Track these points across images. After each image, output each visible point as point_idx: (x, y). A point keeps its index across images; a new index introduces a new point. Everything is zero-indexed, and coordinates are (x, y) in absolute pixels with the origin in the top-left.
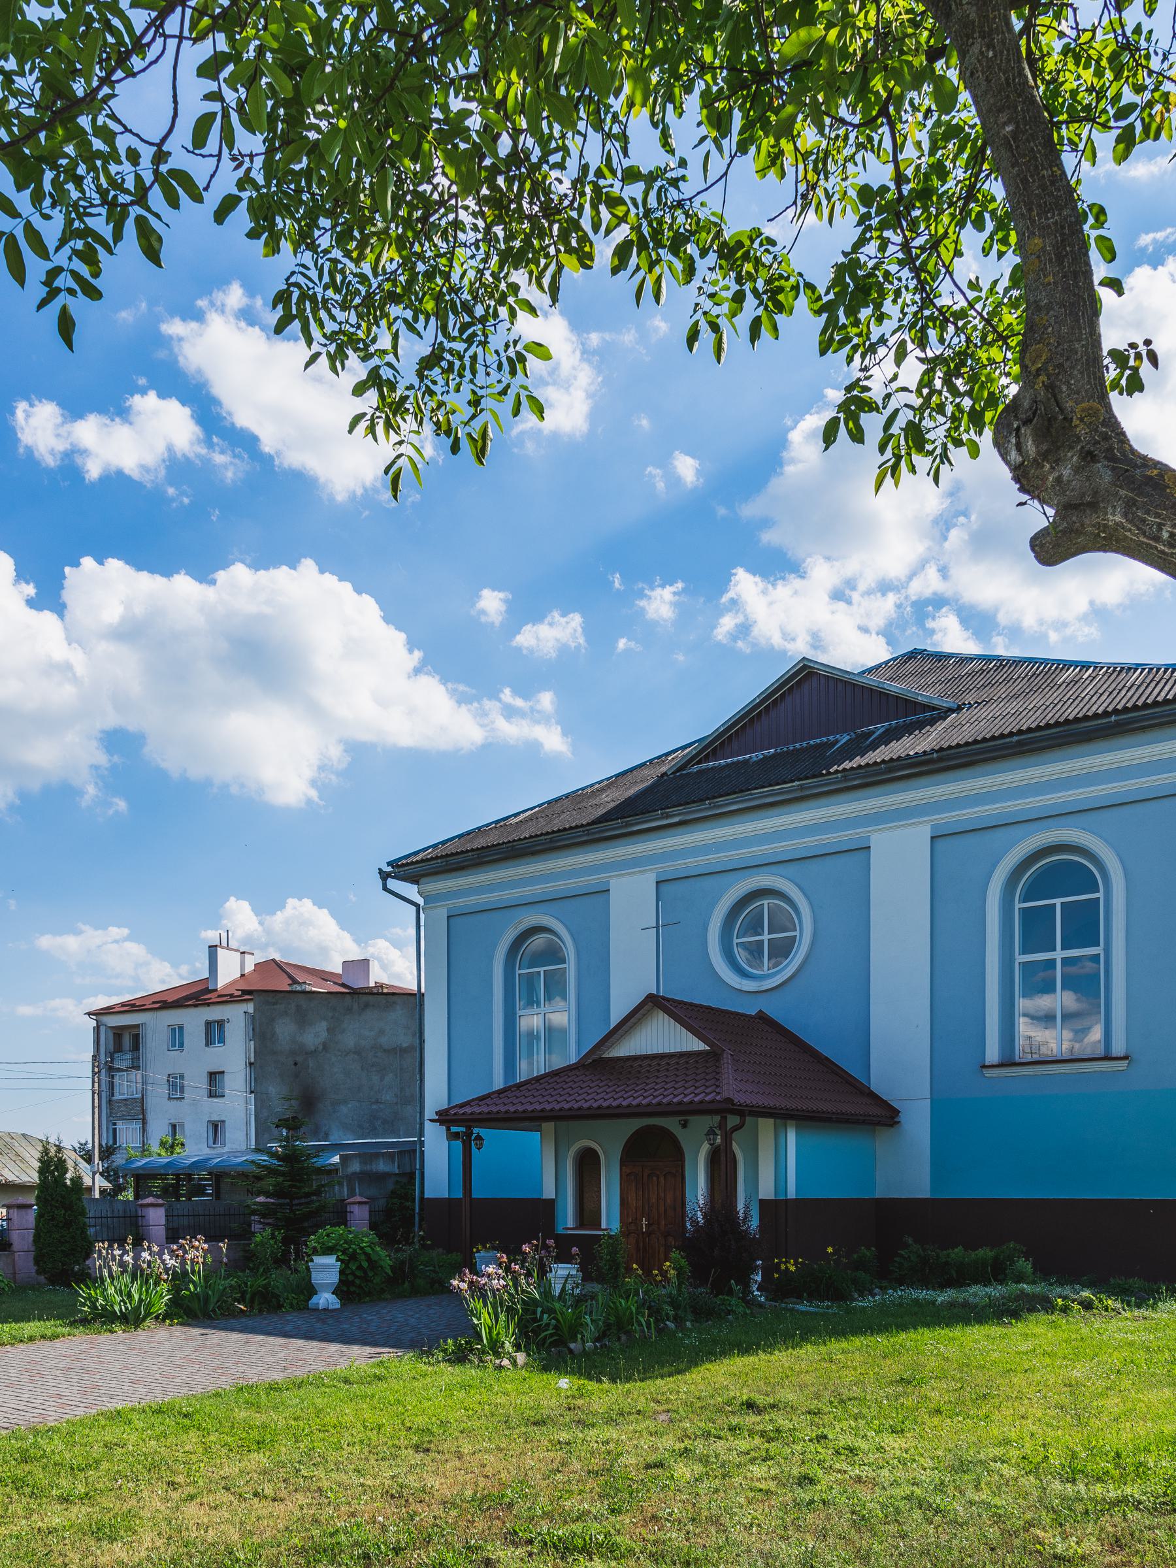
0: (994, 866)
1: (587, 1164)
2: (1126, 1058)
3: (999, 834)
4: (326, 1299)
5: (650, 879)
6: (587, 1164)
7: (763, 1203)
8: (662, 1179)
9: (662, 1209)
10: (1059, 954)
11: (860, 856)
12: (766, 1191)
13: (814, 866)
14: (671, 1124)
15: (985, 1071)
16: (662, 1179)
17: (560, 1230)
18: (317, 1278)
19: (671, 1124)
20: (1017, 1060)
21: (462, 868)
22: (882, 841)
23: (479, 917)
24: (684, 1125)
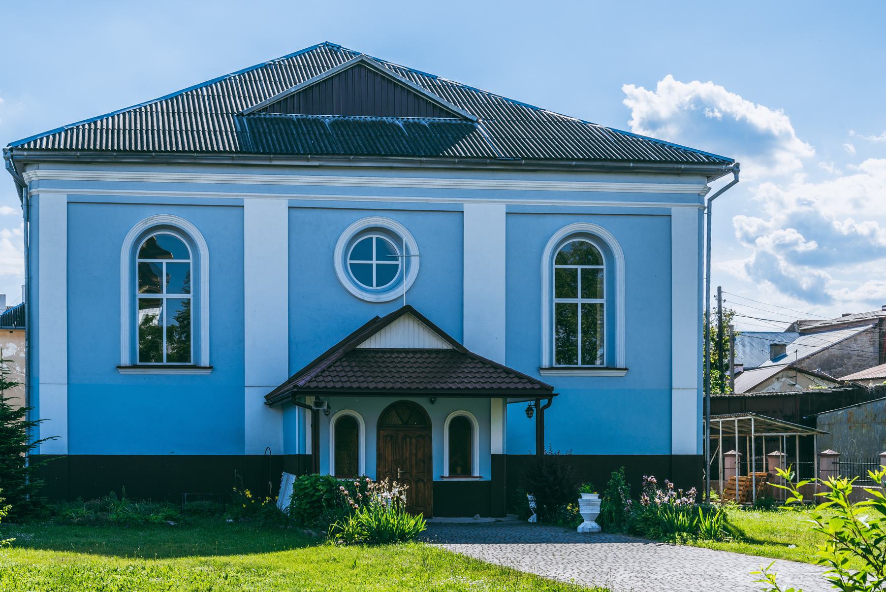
0: (547, 242)
1: (347, 431)
2: (626, 369)
3: (549, 219)
4: (588, 525)
5: (64, 199)
6: (347, 431)
7: (495, 458)
8: (414, 440)
9: (414, 462)
10: (579, 301)
11: (236, 211)
12: (498, 446)
13: (420, 217)
14: (423, 402)
15: (541, 372)
16: (414, 440)
17: (435, 478)
18: (584, 510)
19: (423, 402)
20: (618, 367)
21: (591, 172)
22: (253, 206)
23: (119, 207)
24: (432, 402)
